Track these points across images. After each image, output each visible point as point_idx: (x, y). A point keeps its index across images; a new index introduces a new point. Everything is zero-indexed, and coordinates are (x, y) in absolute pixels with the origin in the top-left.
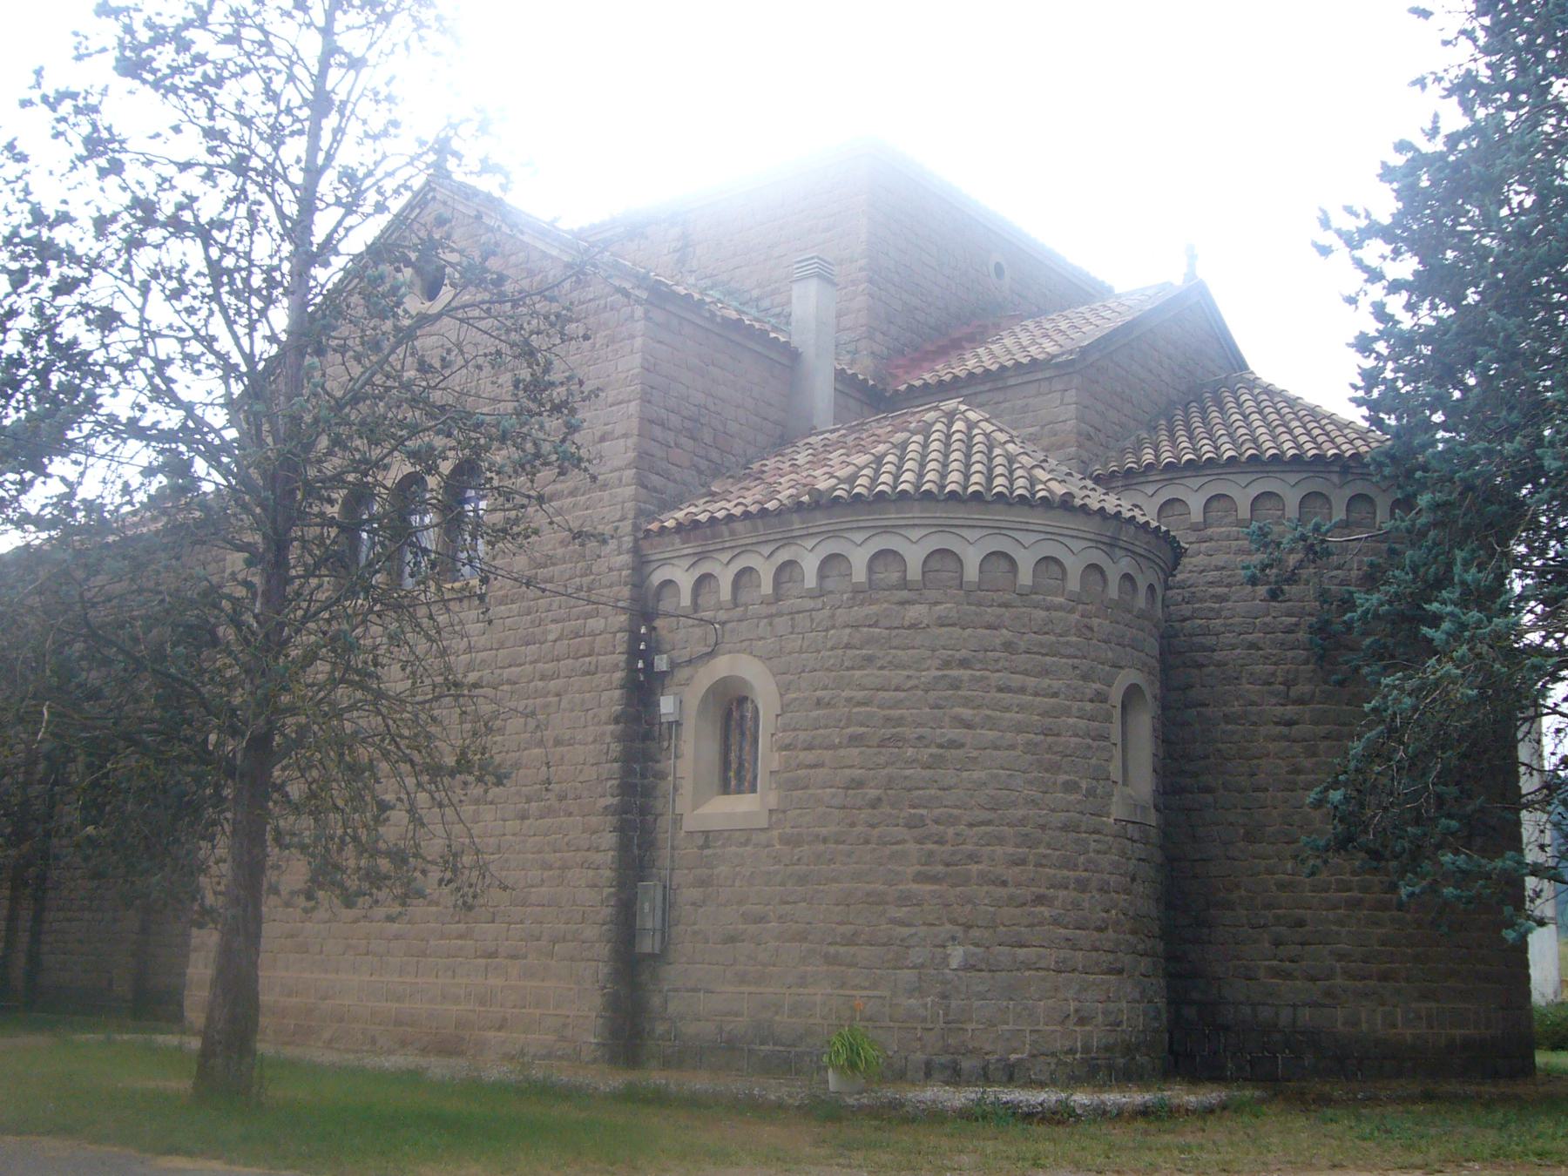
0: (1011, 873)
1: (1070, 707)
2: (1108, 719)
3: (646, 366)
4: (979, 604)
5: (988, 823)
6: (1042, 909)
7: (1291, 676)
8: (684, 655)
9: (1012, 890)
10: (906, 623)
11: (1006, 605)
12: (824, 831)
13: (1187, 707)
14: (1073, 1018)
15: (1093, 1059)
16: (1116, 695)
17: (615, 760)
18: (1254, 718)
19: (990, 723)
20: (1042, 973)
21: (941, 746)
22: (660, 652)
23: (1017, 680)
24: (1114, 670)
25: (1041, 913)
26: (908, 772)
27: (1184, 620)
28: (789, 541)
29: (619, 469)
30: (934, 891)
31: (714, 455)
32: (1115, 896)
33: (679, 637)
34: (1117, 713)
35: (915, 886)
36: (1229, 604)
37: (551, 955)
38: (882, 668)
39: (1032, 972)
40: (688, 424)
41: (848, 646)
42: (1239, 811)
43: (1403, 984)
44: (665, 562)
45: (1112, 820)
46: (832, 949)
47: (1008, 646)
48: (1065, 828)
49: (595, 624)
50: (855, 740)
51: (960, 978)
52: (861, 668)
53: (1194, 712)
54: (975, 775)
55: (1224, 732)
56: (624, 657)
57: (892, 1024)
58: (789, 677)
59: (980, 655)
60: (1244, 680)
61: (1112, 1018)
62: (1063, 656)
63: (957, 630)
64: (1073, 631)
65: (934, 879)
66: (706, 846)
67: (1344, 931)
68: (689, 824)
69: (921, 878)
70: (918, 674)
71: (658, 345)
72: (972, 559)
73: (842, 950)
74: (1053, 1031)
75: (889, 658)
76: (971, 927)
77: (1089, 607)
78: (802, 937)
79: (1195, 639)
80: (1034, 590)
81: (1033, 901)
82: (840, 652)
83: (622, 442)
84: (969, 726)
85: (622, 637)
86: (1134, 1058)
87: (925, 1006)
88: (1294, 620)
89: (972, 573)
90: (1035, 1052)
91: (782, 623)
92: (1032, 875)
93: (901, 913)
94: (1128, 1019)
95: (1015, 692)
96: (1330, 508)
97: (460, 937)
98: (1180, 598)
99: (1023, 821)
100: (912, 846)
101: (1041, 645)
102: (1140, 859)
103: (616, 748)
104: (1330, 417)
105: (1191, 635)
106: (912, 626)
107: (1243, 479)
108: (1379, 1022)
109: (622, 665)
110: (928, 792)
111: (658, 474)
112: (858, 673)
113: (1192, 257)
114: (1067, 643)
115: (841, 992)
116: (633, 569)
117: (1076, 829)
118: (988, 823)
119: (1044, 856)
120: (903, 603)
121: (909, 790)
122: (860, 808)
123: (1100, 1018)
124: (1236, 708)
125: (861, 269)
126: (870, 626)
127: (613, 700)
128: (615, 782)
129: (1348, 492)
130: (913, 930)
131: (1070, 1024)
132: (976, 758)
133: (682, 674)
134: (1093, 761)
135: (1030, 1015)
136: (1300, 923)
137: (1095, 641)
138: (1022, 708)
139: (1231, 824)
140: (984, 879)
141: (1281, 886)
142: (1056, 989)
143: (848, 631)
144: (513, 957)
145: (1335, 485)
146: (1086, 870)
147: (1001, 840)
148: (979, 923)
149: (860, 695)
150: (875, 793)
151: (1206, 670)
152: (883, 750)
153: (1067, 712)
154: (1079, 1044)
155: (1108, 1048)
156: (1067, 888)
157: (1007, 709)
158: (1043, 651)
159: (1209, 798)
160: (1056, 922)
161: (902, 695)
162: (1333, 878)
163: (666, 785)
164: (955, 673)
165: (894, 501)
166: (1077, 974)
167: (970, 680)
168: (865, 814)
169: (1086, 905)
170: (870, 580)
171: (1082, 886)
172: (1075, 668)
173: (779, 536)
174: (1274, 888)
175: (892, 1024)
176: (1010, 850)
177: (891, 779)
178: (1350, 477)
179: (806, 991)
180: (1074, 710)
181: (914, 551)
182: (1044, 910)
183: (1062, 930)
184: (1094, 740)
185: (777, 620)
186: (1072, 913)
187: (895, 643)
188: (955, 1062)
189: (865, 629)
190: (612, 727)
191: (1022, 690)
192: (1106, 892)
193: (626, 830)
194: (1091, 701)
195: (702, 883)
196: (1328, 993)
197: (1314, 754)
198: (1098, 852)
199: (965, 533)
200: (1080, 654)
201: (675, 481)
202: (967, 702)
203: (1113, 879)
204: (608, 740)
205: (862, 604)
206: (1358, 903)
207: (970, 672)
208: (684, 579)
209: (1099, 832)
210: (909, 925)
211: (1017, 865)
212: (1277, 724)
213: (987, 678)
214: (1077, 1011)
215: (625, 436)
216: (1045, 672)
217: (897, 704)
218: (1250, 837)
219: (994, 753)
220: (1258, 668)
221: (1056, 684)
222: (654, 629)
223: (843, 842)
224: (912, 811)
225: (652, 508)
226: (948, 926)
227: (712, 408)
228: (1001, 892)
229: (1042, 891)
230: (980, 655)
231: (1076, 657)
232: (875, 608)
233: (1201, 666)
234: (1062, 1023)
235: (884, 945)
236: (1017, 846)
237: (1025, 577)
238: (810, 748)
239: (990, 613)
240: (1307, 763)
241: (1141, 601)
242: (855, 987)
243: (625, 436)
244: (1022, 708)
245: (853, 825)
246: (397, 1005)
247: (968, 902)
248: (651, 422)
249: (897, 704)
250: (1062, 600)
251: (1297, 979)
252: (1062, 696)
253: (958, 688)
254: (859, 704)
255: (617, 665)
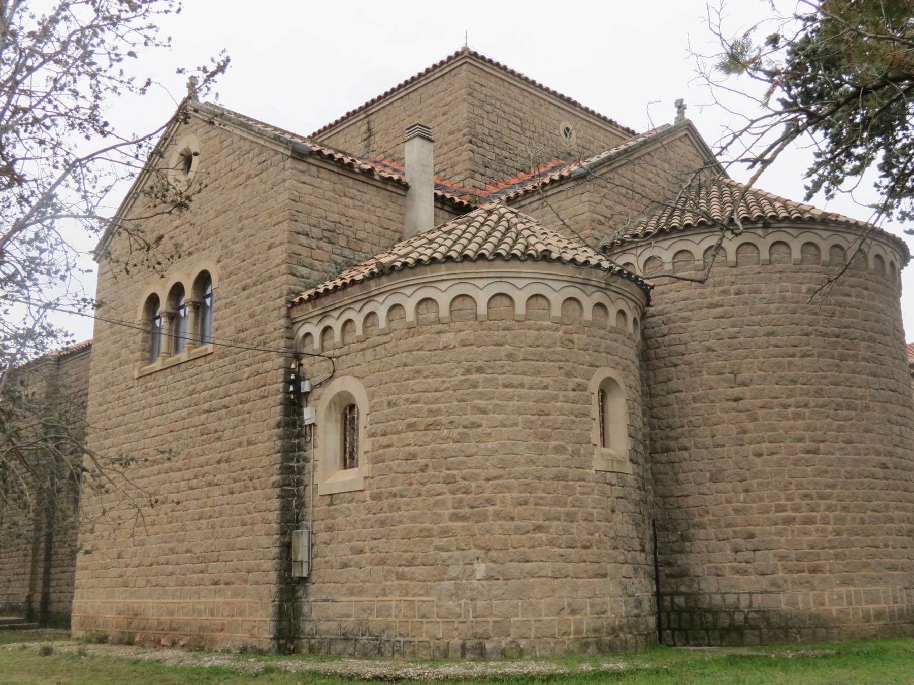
0: (516, 511)
1: (557, 395)
2: (588, 402)
3: (293, 197)
4: (489, 329)
5: (500, 477)
6: (541, 535)
7: (736, 368)
8: (317, 380)
9: (517, 523)
10: (441, 346)
11: (508, 329)
12: (394, 489)
13: (668, 393)
14: (567, 611)
15: (583, 638)
16: (594, 386)
17: (278, 452)
18: (712, 398)
19: (499, 409)
20: (543, 580)
21: (465, 427)
22: (304, 379)
23: (516, 379)
24: (592, 368)
25: (541, 538)
26: (444, 446)
27: (664, 336)
28: (369, 299)
29: (278, 265)
30: (463, 526)
31: (347, 252)
32: (599, 523)
33: (313, 368)
34: (595, 399)
35: (451, 524)
36: (693, 323)
37: (246, 581)
38: (427, 377)
39: (536, 580)
40: (326, 234)
41: (405, 365)
42: (706, 461)
43: (828, 575)
44: (306, 321)
45: (593, 471)
46: (400, 569)
47: (510, 356)
48: (556, 478)
49: (268, 365)
50: (411, 427)
51: (483, 586)
52: (414, 378)
53: (673, 395)
54: (489, 445)
55: (692, 409)
56: (282, 385)
57: (438, 619)
58: (373, 388)
59: (491, 364)
60: (705, 373)
61: (598, 609)
62: (551, 361)
63: (475, 347)
64: (558, 343)
65: (464, 518)
66: (331, 504)
67: (783, 540)
68: (322, 490)
69: (455, 517)
70: (449, 379)
71: (301, 185)
72: (482, 300)
73: (406, 569)
74: (552, 620)
75: (431, 371)
76: (489, 550)
77: (570, 327)
78: (382, 562)
79: (672, 348)
80: (527, 318)
81: (534, 530)
82: (401, 369)
83: (279, 248)
84: (485, 412)
85: (282, 371)
86: (618, 636)
87: (460, 605)
88: (736, 329)
89: (482, 309)
90: (539, 635)
91: (369, 354)
92: (532, 512)
93: (443, 542)
94: (612, 609)
95: (516, 387)
96: (758, 252)
97: (201, 572)
98: (660, 322)
99: (524, 475)
100: (449, 496)
101: (534, 354)
102: (618, 498)
103: (279, 443)
104: (777, 199)
105: (669, 345)
106: (445, 348)
107: (697, 239)
108: (812, 601)
109: (281, 390)
110: (457, 459)
111: (304, 266)
112: (411, 382)
113: (681, 106)
114: (554, 352)
115: (406, 598)
116: (287, 328)
117: (565, 478)
118: (500, 477)
119: (541, 498)
120: (439, 333)
121: (446, 458)
122: (415, 473)
123: (588, 609)
124: (701, 392)
125: (464, 135)
126: (419, 350)
127: (276, 414)
128: (278, 466)
129: (770, 240)
130: (450, 554)
131: (565, 615)
132: (489, 434)
133: (317, 392)
134: (577, 431)
135: (534, 610)
136: (751, 536)
137: (576, 350)
138: (521, 398)
139: (701, 470)
140: (497, 516)
141: (737, 511)
142: (554, 590)
143: (405, 354)
144: (227, 584)
145: (760, 236)
146: (574, 506)
147: (509, 489)
148: (495, 547)
149: (413, 396)
150: (424, 461)
151: (679, 368)
152: (428, 432)
153: (555, 398)
154: (572, 629)
155: (596, 630)
156: (559, 519)
157: (511, 399)
158: (536, 358)
159: (685, 454)
160: (551, 543)
161: (438, 394)
162: (772, 504)
163: (309, 466)
164: (474, 376)
165: (428, 265)
166: (569, 579)
167: (484, 381)
168: (416, 477)
169: (574, 530)
170: (417, 320)
171: (571, 518)
172: (560, 368)
173: (364, 297)
174: (732, 512)
175: (438, 619)
176: (515, 495)
177: (433, 451)
178: (770, 230)
179: (386, 598)
180: (561, 398)
181: (443, 297)
182: (543, 536)
183: (556, 549)
184: (577, 416)
185: (367, 352)
186: (564, 537)
187: (434, 359)
188: (481, 644)
189: (415, 352)
190: (276, 430)
191: (521, 385)
192: (590, 521)
193: (285, 496)
194: (574, 390)
195: (330, 529)
196: (774, 584)
197: (756, 419)
198: (583, 493)
199: (476, 282)
200: (563, 359)
201: (318, 271)
202: (482, 396)
203: (595, 512)
204: (275, 439)
205: (413, 336)
206: (789, 521)
207: (484, 375)
208: (315, 330)
209: (583, 480)
210: (448, 550)
211: (521, 505)
212: (728, 400)
213: (496, 379)
214: (569, 605)
215: (281, 243)
216: (538, 372)
217: (437, 400)
218: (714, 479)
219: (504, 429)
220: (713, 364)
221: (546, 380)
222: (301, 365)
223: (405, 496)
224: (448, 472)
225: (300, 288)
226: (475, 550)
227: (345, 223)
228: (512, 524)
229: (541, 522)
230: (491, 364)
231: (561, 361)
232: (421, 338)
233: (676, 366)
234: (558, 613)
235: (432, 565)
236: (521, 492)
237: (520, 309)
238: (384, 435)
239: (497, 335)
240: (750, 426)
241: (612, 320)
242: (415, 595)
243: (281, 243)
244: (521, 398)
245: (411, 484)
246: (875, 606)
247: (488, 532)
248: (298, 233)
249: (437, 400)
250: (549, 323)
251: (751, 574)
252: (550, 388)
253: (476, 387)
254: (413, 402)
255: (278, 390)
